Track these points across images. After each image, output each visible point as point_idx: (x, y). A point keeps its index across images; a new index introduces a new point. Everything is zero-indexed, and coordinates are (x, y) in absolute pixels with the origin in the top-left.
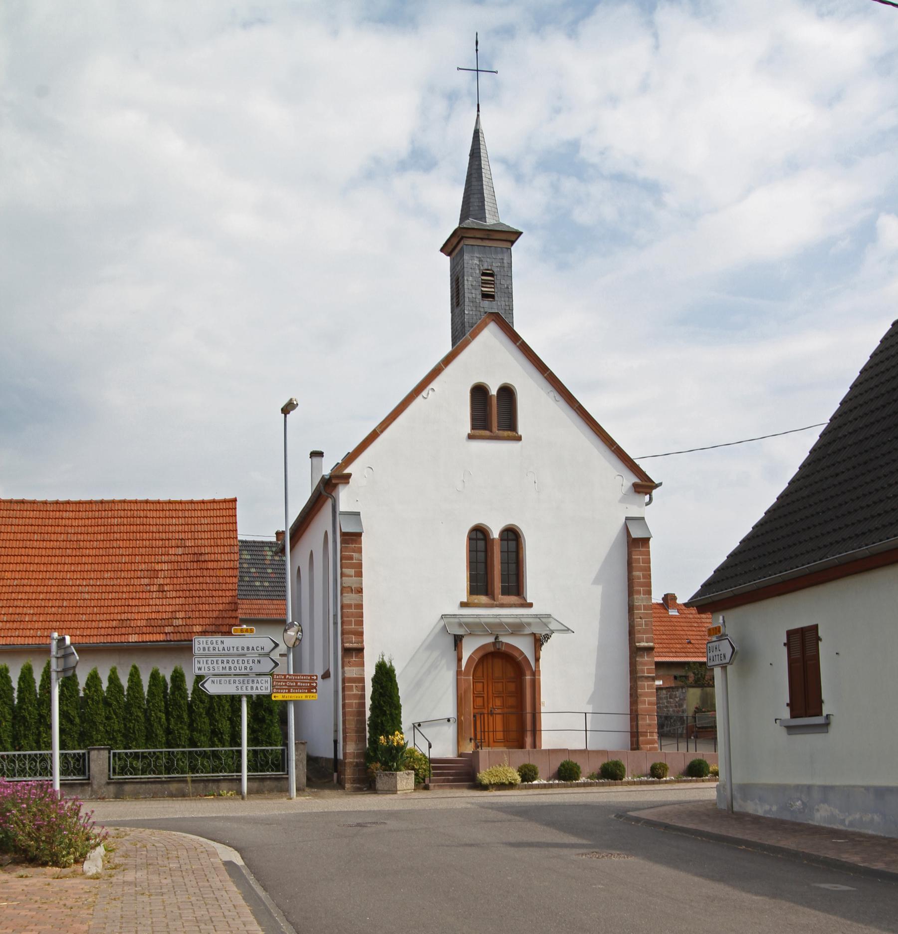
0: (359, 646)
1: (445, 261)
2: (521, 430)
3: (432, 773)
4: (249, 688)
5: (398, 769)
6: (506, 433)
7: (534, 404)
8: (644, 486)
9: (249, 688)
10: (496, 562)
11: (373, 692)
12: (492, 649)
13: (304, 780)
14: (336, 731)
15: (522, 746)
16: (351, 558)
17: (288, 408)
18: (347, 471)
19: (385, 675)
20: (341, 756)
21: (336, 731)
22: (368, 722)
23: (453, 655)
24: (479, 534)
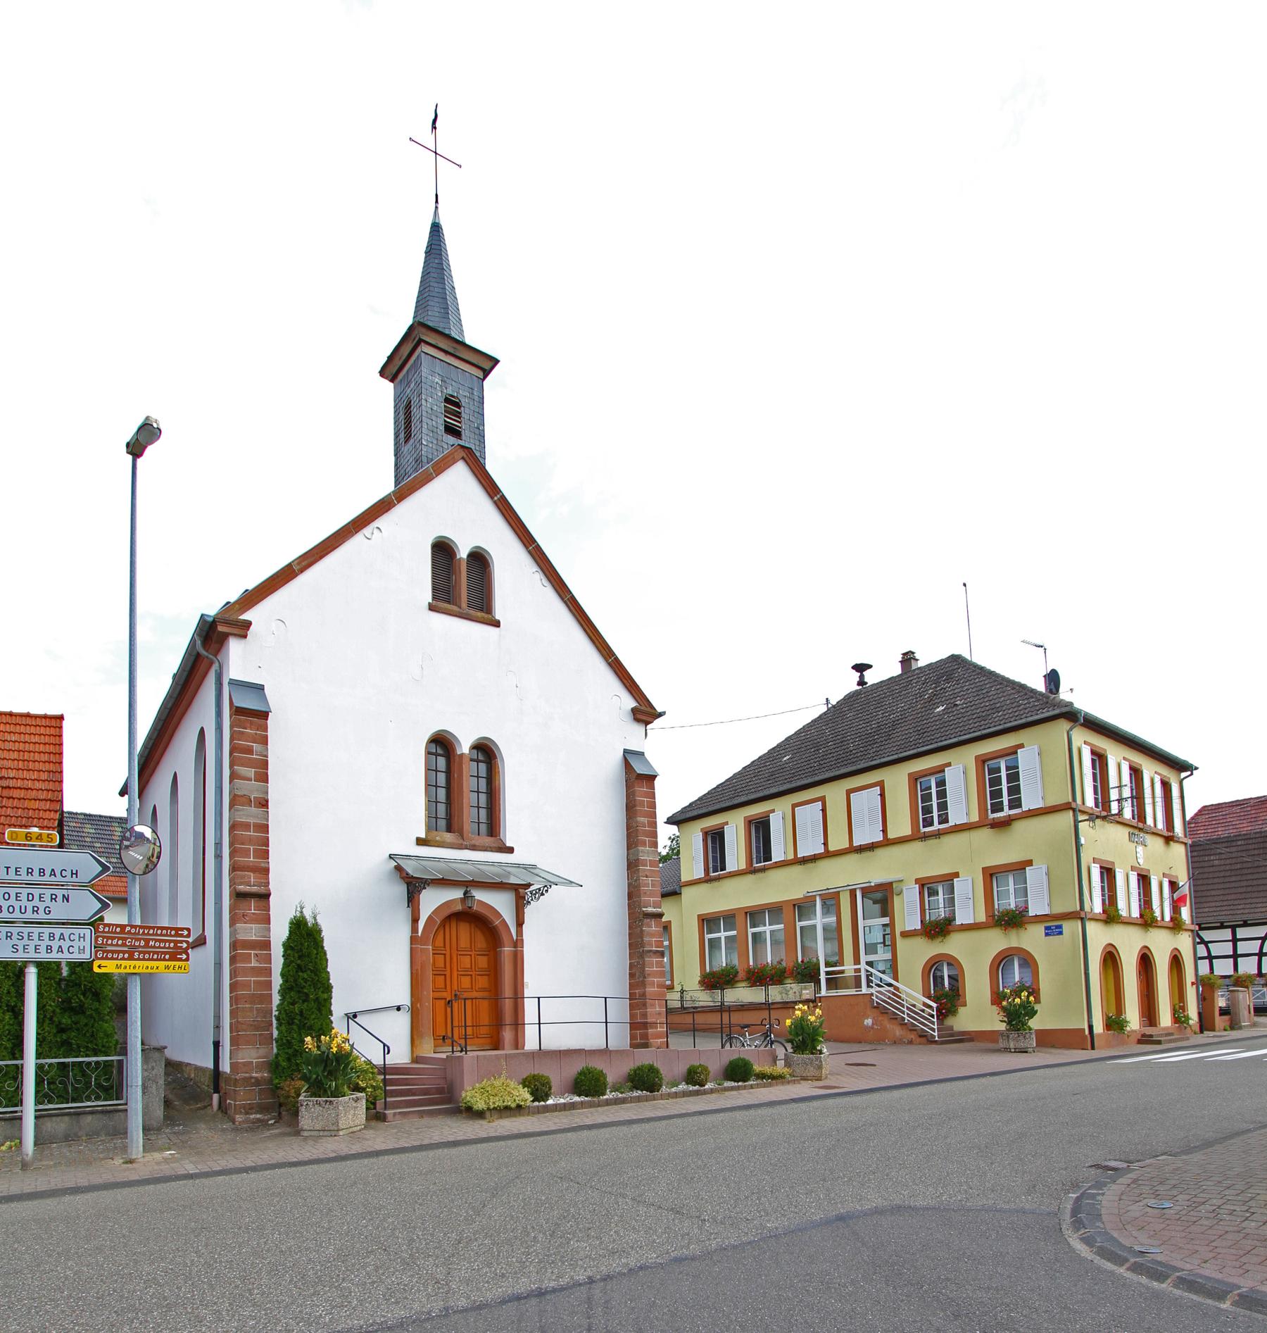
0: (262, 890)
1: (387, 389)
2: (498, 614)
3: (388, 1092)
4: (43, 949)
5: (337, 1093)
6: (480, 614)
7: (512, 576)
8: (645, 713)
9: (43, 949)
10: (464, 782)
11: (286, 965)
12: (459, 907)
13: (159, 1112)
14: (217, 1027)
15: (497, 1045)
16: (249, 751)
17: (142, 440)
18: (245, 617)
19: (305, 938)
20: (225, 1067)
21: (217, 1027)
22: (275, 1013)
23: (404, 914)
24: (441, 744)
